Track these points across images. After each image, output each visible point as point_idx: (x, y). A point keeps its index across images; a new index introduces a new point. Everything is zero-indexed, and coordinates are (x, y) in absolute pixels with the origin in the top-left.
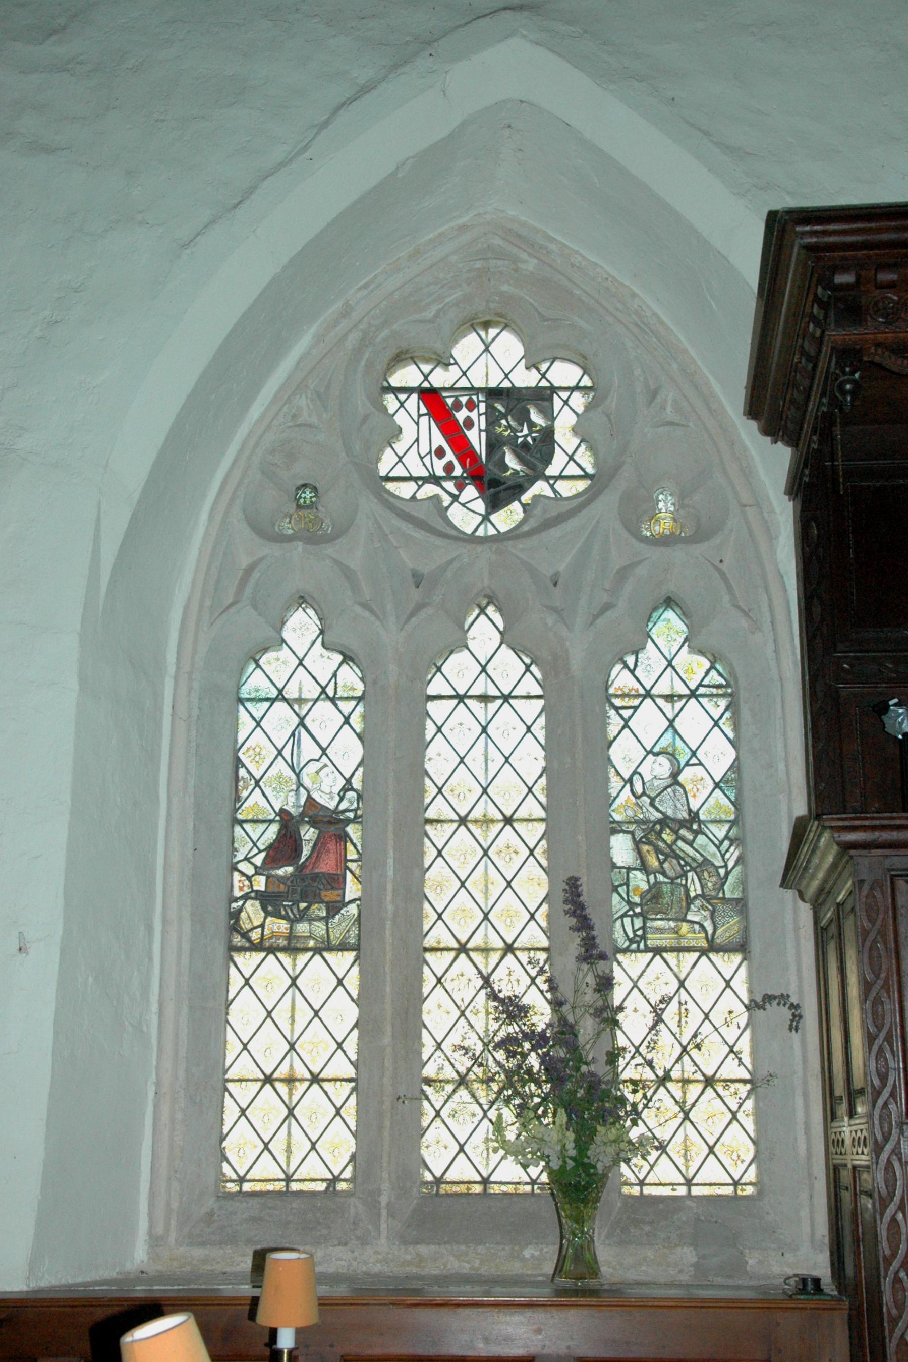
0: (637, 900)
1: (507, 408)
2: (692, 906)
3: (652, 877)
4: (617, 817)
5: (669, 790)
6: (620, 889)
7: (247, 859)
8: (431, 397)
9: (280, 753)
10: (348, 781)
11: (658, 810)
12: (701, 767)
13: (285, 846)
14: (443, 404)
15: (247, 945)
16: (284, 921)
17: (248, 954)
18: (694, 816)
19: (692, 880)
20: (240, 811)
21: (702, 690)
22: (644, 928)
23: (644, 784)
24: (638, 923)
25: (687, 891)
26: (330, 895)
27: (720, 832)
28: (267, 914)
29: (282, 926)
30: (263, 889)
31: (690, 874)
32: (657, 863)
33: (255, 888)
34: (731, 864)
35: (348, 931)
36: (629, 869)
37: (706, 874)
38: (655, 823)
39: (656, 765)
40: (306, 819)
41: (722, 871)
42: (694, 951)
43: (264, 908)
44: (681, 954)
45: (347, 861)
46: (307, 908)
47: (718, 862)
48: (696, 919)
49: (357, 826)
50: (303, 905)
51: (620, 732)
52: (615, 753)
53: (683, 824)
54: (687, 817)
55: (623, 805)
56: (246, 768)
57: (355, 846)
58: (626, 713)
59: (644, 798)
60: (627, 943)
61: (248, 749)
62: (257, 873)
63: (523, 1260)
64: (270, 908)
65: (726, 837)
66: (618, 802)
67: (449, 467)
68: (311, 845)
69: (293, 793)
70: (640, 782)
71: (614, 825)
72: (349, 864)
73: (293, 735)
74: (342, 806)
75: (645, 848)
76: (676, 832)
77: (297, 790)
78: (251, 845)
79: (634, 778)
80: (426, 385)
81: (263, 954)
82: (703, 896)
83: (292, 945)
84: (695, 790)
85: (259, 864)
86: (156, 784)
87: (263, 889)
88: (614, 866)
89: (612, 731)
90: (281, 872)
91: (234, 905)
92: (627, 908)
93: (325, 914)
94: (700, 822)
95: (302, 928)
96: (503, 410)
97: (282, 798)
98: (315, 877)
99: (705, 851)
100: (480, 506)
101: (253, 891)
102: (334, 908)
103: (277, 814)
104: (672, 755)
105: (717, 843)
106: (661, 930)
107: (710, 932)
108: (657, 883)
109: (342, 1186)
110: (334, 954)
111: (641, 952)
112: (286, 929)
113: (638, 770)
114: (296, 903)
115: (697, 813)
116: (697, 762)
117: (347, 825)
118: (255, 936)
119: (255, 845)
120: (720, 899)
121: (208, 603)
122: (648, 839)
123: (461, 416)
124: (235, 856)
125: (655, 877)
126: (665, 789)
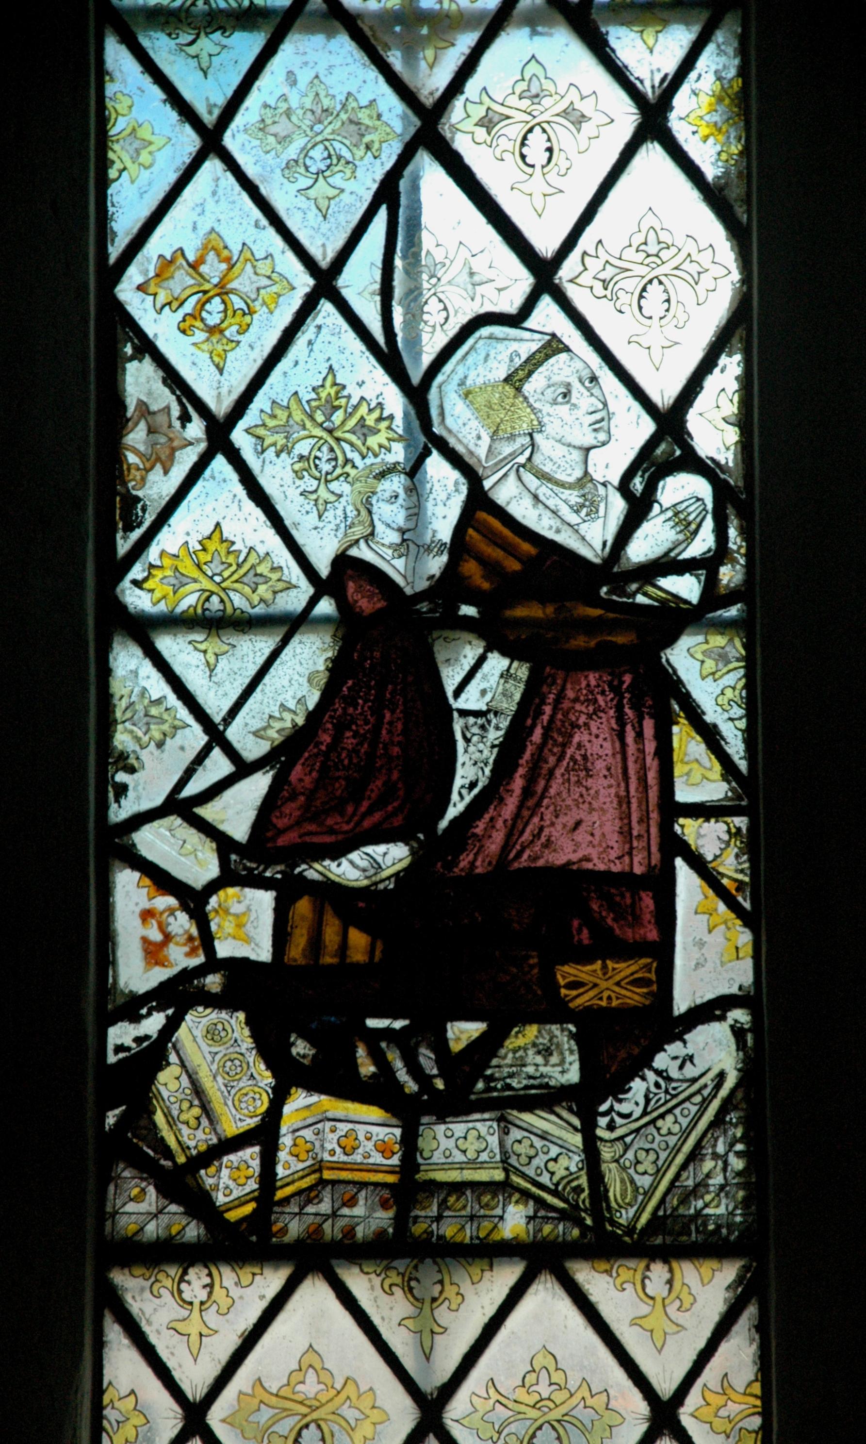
7: (179, 806)
9: (326, 283)
10: (670, 421)
15: (193, 1231)
16: (374, 1113)
17: (197, 1277)
20: (137, 572)
26: (601, 983)
28: (288, 1077)
29: (363, 1134)
30: (263, 953)
33: (224, 950)
35: (695, 1156)
40: (468, 610)
43: (271, 1049)
45: (674, 811)
46: (485, 1048)
49: (718, 641)
50: (463, 1032)
56: (161, 361)
57: (711, 736)
61: (166, 265)
62: (228, 878)
64: (301, 1048)
68: (494, 735)
69: (396, 483)
72: (689, 829)
73: (388, 193)
74: (642, 548)
77: (414, 468)
78: (196, 737)
81: (272, 1281)
83: (418, 1229)
85: (240, 831)
87: (263, 953)
90: (348, 870)
91: (122, 1034)
93: (573, 1075)
95: (459, 1145)
97: (347, 506)
101: (213, 963)
102: (626, 1040)
103: (321, 587)
110: (628, 1270)
112: (384, 1149)
117: (671, 640)
118: (231, 1183)
119: (216, 736)
124: (122, 790)
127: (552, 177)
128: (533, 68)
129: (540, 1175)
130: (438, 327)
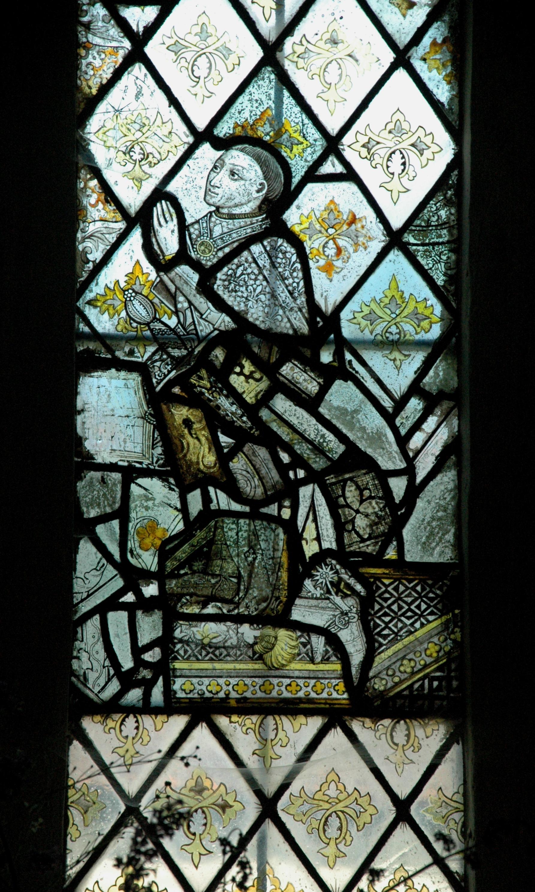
0: (148, 560)
2: (308, 583)
3: (195, 500)
4: (103, 323)
5: (256, 249)
6: (100, 529)
11: (221, 305)
12: (350, 187)
18: (325, 324)
19: (312, 507)
22: (165, 642)
23: (183, 227)
24: (150, 627)
25: (295, 538)
27: (397, 373)
31: (305, 492)
32: (211, 459)
34: (424, 465)
36: (130, 473)
37: (351, 493)
38: (212, 343)
39: (222, 177)
41: (398, 486)
42: (309, 713)
44: (270, 720)
47: (389, 459)
48: (319, 619)
51: (118, 74)
52: (104, 135)
53: (294, 347)
54: (305, 329)
55: (118, 278)
59: (184, 270)
60: (114, 686)
65: (415, 389)
66: (110, 276)
70: (173, 224)
71: (92, 346)
75: (180, 413)
76: (270, 370)
79: (157, 210)
82: (341, 555)
84: (331, 251)
86: (309, 708)
88: (88, 463)
89: (97, 66)
92: (119, 583)
94: (342, 344)
99: (351, 426)
104: (268, 148)
105: (387, 403)
106: (212, 650)
107: (357, 658)
108: (209, 514)
111: (156, 711)
113: (171, 188)
115: (333, 320)
116: (339, 169)
120: (389, 564)
122: (188, 387)
125: (206, 499)
126: (245, 244)
127: (404, 180)
128: (398, 116)
129: (331, 695)
130: (138, 162)
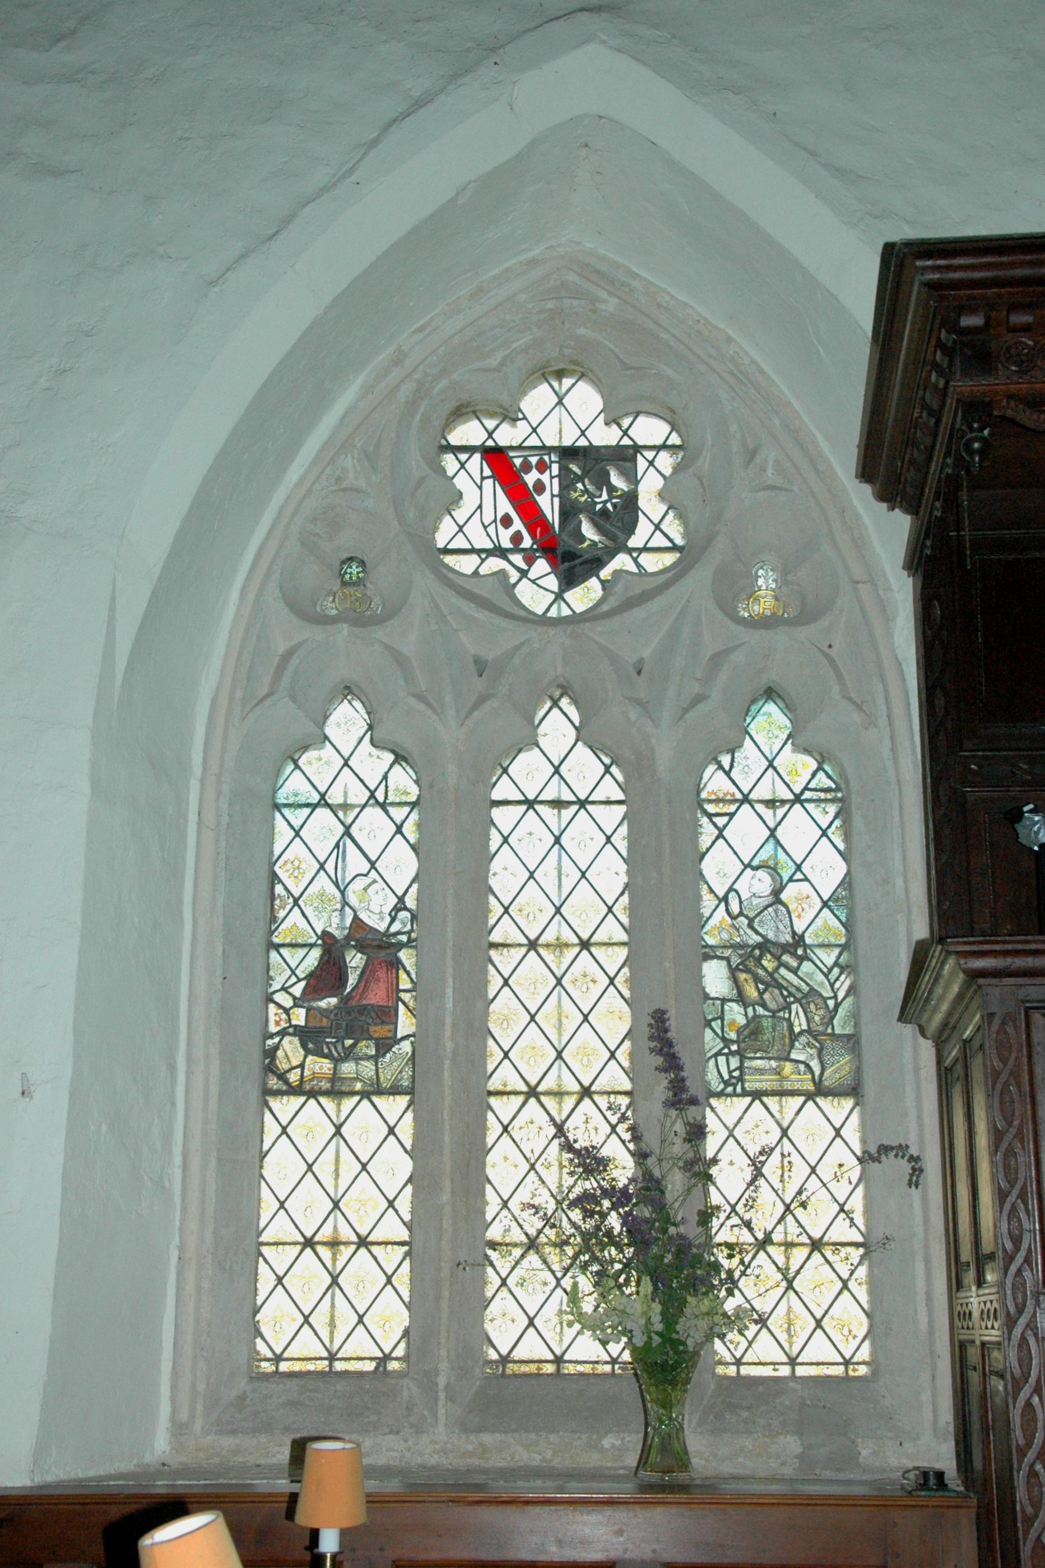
0: (733, 1036)
1: (583, 469)
2: (797, 1043)
3: (750, 1010)
4: (711, 941)
5: (770, 909)
6: (713, 1024)
7: (284, 989)
8: (496, 457)
9: (322, 867)
10: (401, 899)
11: (757, 932)
12: (806, 883)
13: (328, 975)
14: (510, 465)
15: (285, 1088)
16: (327, 1061)
17: (285, 1098)
18: (799, 940)
19: (797, 1013)
20: (276, 934)
21: (807, 795)
22: (741, 1068)
23: (741, 902)
24: (735, 1062)
25: (791, 1026)
26: (380, 1031)
27: (829, 958)
28: (308, 1052)
29: (325, 1066)
30: (303, 1023)
31: (794, 1007)
32: (756, 994)
33: (294, 1022)
34: (841, 995)
35: (401, 1072)
36: (724, 1001)
37: (812, 1006)
38: (754, 947)
39: (755, 881)
40: (353, 943)
41: (831, 1003)
42: (799, 1095)
43: (304, 1046)
44: (784, 1098)
45: (399, 991)
46: (354, 1046)
47: (827, 993)
48: (802, 1058)
49: (410, 951)
50: (349, 1042)
51: (713, 843)
52: (708, 867)
53: (786, 948)
54: (791, 940)
55: (717, 927)
56: (283, 885)
57: (408, 973)
58: (720, 821)
59: (742, 919)
60: (722, 1086)
61: (286, 862)
62: (295, 1005)
63: (602, 1450)
64: (310, 1046)
65: (836, 964)
66: (711, 923)
67: (517, 538)
68: (358, 973)
69: (337, 913)
70: (737, 901)
71: (707, 950)
72: (402, 995)
73: (337, 846)
74: (394, 928)
75: (742, 976)
76: (778, 958)
77: (342, 910)
78: (289, 972)
79: (730, 896)
80: (490, 443)
81: (303, 1099)
82: (809, 1031)
83: (336, 1088)
84: (800, 909)
85: (298, 994)
86: (180, 903)
87: (303, 1023)
88: (707, 997)
89: (705, 841)
90: (323, 1004)
91: (270, 1042)
92: (722, 1045)
93: (373, 1053)
94: (805, 947)
95: (348, 1068)
96: (579, 472)
97: (325, 918)
98: (363, 1010)
99: (811, 979)
100: (552, 583)
101: (291, 1026)
102: (385, 1046)
103: (319, 938)
104: (773, 869)
105: (825, 970)
106: (760, 1071)
107: (817, 1073)
108: (756, 1016)
109: (393, 1366)
110: (384, 1098)
111: (738, 1096)
112: (329, 1069)
113: (735, 887)
114: (341, 1040)
115: (802, 936)
116: (802, 877)
117: (400, 950)
118: (294, 1077)
119: (293, 972)
120: (828, 1035)
121: (239, 694)
122: (746, 966)
123: (530, 479)
124: (271, 985)
125: (754, 1010)
126: (766, 908)
